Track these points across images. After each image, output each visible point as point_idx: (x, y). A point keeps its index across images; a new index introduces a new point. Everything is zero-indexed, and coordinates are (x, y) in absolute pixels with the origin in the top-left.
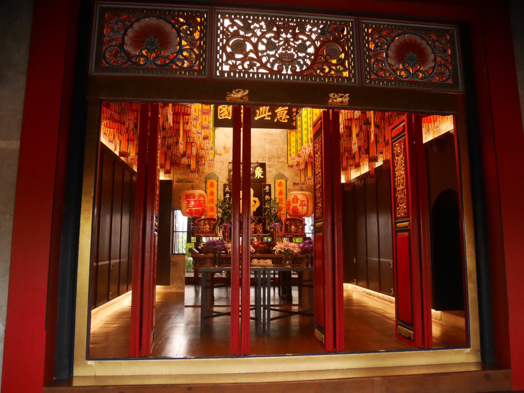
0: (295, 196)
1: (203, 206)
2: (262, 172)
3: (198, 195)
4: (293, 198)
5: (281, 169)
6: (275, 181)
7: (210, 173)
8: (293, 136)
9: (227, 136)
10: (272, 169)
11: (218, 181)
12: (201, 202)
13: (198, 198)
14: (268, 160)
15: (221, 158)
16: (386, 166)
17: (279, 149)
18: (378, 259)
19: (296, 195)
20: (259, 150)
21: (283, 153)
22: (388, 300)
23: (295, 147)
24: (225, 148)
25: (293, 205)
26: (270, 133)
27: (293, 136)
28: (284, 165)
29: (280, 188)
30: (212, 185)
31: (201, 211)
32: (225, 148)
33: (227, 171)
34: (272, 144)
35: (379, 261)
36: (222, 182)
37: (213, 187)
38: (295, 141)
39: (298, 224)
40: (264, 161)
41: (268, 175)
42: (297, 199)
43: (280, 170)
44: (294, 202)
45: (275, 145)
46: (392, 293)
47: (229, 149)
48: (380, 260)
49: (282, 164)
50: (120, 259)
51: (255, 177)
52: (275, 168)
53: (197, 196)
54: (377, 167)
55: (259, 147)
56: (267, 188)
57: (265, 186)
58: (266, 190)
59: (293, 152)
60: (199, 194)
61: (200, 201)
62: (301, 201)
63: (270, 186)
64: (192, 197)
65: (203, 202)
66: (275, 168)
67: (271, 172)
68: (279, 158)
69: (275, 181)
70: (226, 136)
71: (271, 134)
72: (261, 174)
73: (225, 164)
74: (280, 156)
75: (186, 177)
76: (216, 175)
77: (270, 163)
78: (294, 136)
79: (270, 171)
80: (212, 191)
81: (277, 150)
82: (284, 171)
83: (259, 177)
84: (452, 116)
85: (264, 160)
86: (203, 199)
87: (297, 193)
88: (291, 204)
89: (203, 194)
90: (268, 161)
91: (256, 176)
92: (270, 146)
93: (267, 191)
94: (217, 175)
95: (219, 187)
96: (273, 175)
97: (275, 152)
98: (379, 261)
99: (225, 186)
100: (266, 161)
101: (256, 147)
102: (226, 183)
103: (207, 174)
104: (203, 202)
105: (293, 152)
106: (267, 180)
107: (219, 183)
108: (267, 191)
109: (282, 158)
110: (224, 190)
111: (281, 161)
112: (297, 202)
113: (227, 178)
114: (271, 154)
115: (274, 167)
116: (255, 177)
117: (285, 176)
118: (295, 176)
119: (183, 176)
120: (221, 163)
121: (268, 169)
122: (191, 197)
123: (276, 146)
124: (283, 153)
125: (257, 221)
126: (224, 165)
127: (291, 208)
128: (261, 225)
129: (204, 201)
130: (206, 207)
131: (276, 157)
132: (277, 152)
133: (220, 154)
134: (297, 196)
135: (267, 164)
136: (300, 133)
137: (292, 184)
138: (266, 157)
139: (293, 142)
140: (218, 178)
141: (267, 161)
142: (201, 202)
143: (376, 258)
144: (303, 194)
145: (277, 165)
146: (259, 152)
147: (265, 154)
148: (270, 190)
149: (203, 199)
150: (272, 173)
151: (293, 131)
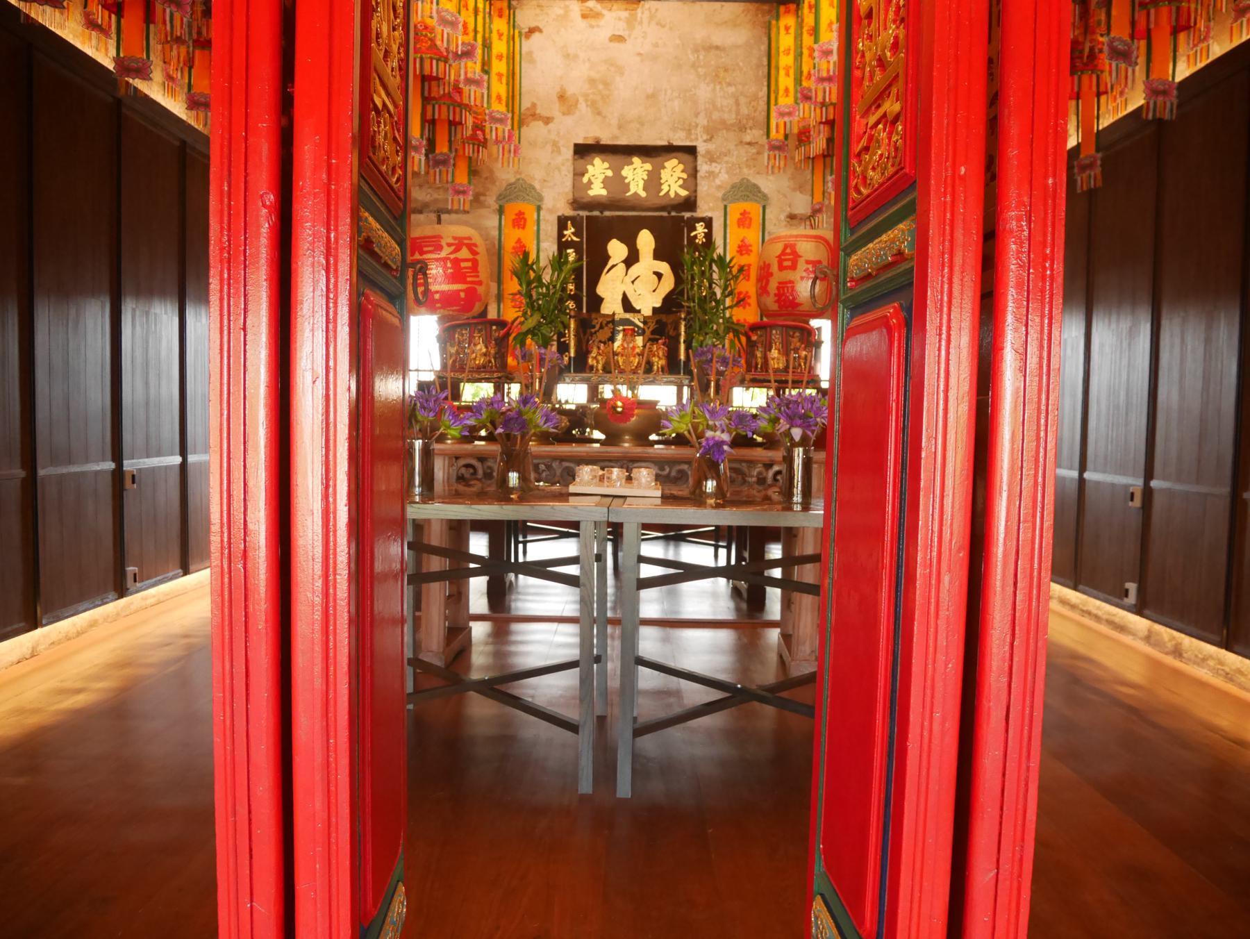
0: (786, 247)
1: (469, 279)
2: (685, 176)
3: (452, 241)
4: (779, 252)
5: (748, 166)
6: (725, 207)
7: (513, 180)
8: (787, 29)
9: (568, 55)
10: (719, 167)
11: (539, 209)
12: (463, 264)
13: (451, 253)
14: (705, 137)
15: (549, 131)
16: (1155, 103)
17: (743, 100)
18: (1075, 474)
19: (792, 240)
20: (676, 103)
21: (755, 111)
22: (1105, 617)
23: (792, 72)
24: (562, 97)
25: (777, 277)
26: (715, 44)
27: (787, 29)
28: (758, 153)
29: (743, 233)
30: (520, 221)
31: (463, 295)
32: (562, 97)
33: (570, 176)
34: (720, 83)
35: (1082, 481)
36: (550, 211)
37: (523, 228)
38: (792, 48)
39: (795, 342)
40: (691, 141)
41: (703, 188)
42: (796, 256)
43: (745, 170)
44: (781, 268)
45: (729, 84)
46: (1132, 599)
47: (577, 101)
48: (1086, 475)
49: (753, 150)
50: (183, 452)
51: (662, 194)
52: (727, 162)
53: (449, 245)
54: (1105, 129)
55: (676, 94)
56: (700, 229)
57: (691, 225)
58: (695, 237)
59: (787, 90)
60: (455, 238)
61: (456, 262)
62: (808, 262)
63: (708, 223)
64: (430, 249)
65: (469, 264)
66: (727, 162)
67: (714, 178)
68: (742, 129)
69: (725, 207)
70: (567, 56)
71: (717, 48)
72: (681, 182)
73: (563, 150)
74: (745, 121)
75: (436, 196)
76: (534, 188)
77: (711, 146)
78: (792, 31)
79: (711, 174)
80: (519, 241)
81: (737, 103)
82: (758, 173)
83: (672, 194)
84: (591, 792)
85: (693, 137)
86: (470, 256)
87: (797, 236)
88: (771, 275)
89: (469, 238)
90: (705, 141)
91: (665, 188)
92: (714, 90)
93: (700, 239)
94: (537, 186)
95: (543, 226)
96: (719, 187)
97: (730, 111)
98: (1082, 481)
99: (562, 223)
100: (697, 139)
101: (666, 91)
102: (566, 214)
103: (504, 185)
104: (469, 264)
105: (787, 90)
106: (700, 203)
107: (542, 213)
108: (700, 239)
109: (751, 129)
110: (560, 235)
111: (748, 138)
112: (794, 267)
113: (570, 197)
114: (716, 115)
115: (726, 159)
116: (662, 194)
117: (760, 191)
118: (794, 190)
119: (430, 190)
120: (549, 148)
121: (703, 167)
122: (425, 249)
123: (732, 89)
124: (755, 111)
125: (653, 333)
126: (559, 152)
127: (773, 286)
128: (664, 344)
129: (475, 263)
130: (480, 283)
131: (732, 125)
132: (734, 108)
133: (548, 118)
134: (793, 247)
135: (702, 148)
136: (813, 10)
137: (782, 217)
138: (697, 125)
139: (787, 52)
140: (541, 198)
141: (700, 140)
142: (463, 264)
143: (1071, 468)
144: (816, 237)
145: (735, 153)
146: (677, 109)
147: (697, 115)
148: (709, 236)
149: (470, 256)
150: (718, 182)
151: (787, 12)
